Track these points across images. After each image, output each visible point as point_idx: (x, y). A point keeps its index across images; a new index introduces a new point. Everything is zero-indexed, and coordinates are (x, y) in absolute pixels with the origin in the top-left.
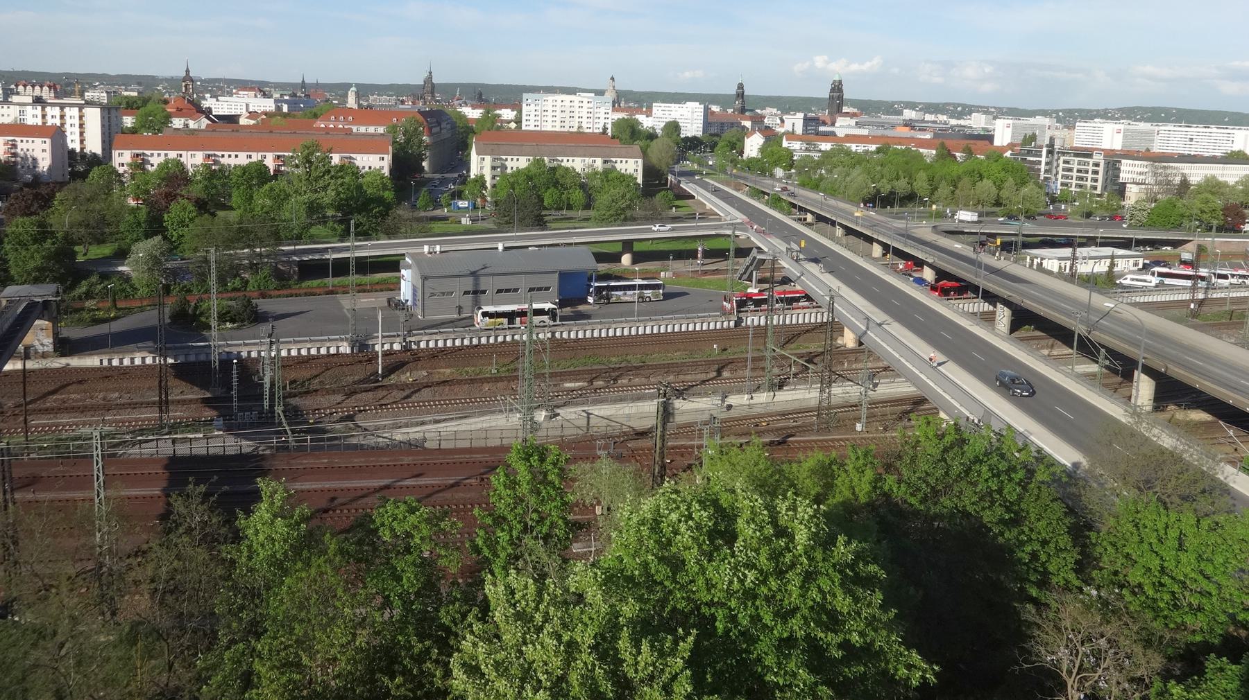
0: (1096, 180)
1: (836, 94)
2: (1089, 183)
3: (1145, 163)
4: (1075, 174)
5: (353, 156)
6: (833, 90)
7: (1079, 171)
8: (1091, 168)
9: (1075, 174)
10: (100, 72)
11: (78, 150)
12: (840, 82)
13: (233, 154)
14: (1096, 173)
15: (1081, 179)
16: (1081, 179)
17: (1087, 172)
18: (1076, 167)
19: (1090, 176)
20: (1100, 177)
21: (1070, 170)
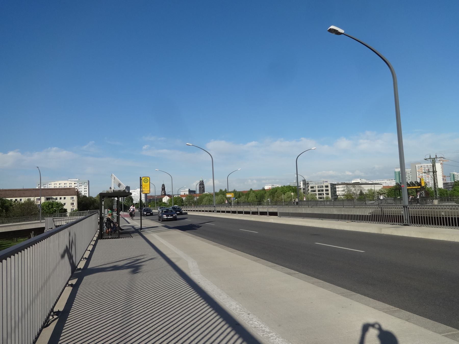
0: (328, 194)
1: (202, 186)
2: (325, 196)
3: (344, 186)
4: (317, 193)
5: (30, 198)
6: (200, 185)
8: (324, 189)
9: (317, 193)
10: (21, 188)
11: (88, 196)
12: (203, 181)
13: (63, 197)
14: (327, 190)
15: (320, 194)
16: (320, 194)
17: (319, 191)
18: (317, 189)
19: (324, 192)
20: (330, 192)
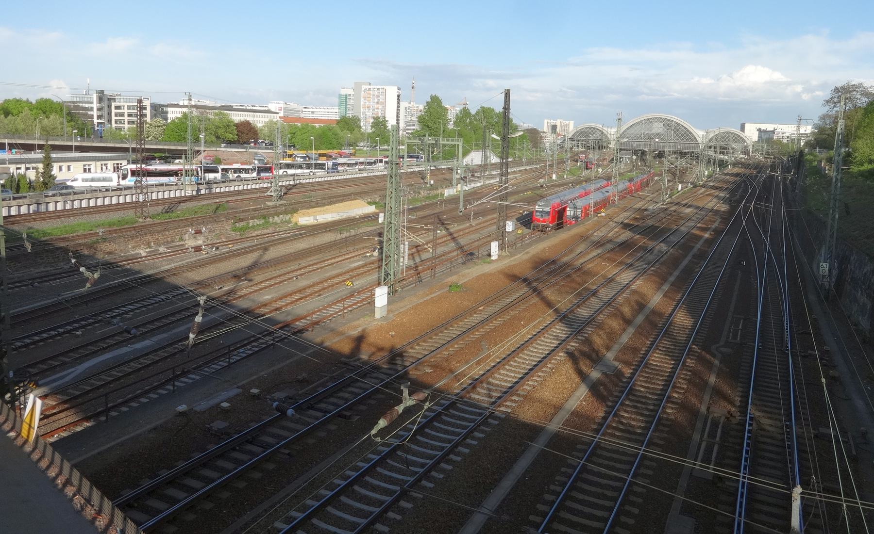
7: (130, 115)
15: (120, 122)
21: (122, 115)
